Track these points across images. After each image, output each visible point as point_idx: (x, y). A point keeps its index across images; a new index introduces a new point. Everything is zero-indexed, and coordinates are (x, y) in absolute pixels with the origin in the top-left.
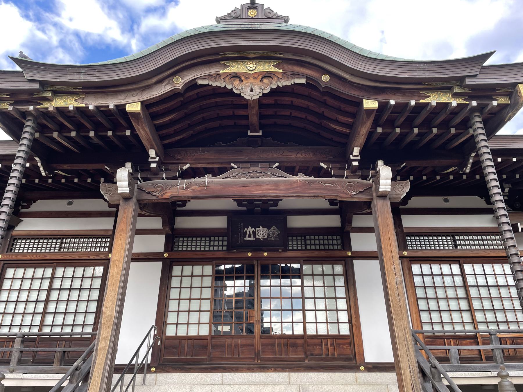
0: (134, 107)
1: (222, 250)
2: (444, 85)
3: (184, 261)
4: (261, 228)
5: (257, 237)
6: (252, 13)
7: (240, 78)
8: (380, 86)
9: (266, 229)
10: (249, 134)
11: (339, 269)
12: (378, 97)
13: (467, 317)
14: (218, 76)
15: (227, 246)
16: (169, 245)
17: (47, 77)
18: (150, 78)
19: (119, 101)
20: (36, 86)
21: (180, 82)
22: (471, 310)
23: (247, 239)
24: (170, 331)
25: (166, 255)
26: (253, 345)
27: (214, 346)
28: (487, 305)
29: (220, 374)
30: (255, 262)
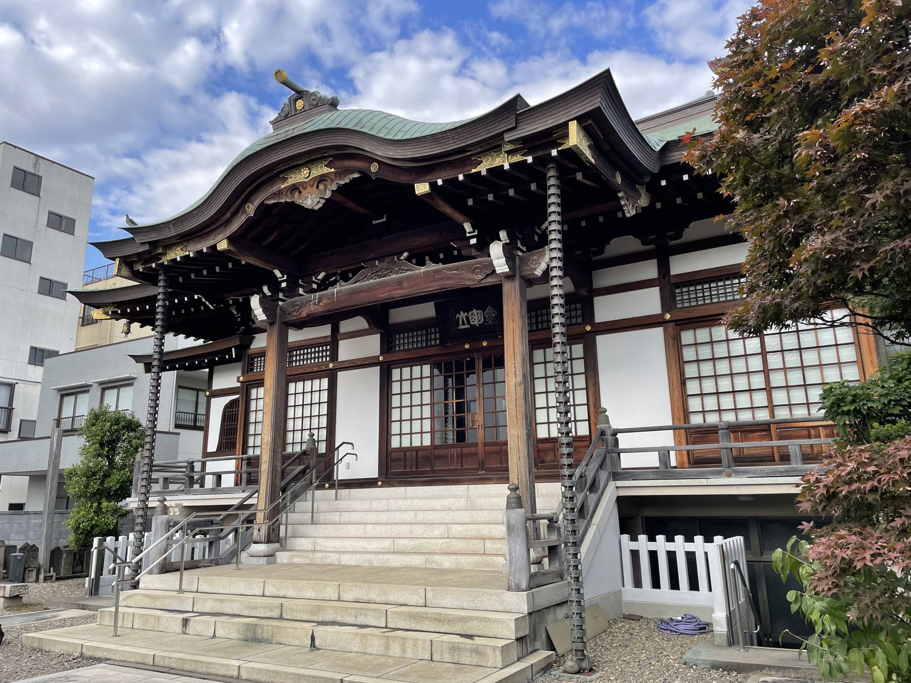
0: (223, 246)
1: (435, 345)
2: (493, 145)
4: (475, 311)
5: (472, 323)
6: (300, 104)
7: (298, 188)
8: (425, 167)
9: (480, 311)
10: (374, 222)
12: (428, 178)
13: (760, 399)
14: (280, 193)
15: (440, 339)
16: (387, 346)
17: (153, 237)
18: (225, 214)
19: (211, 243)
20: (147, 247)
21: (251, 209)
22: (768, 389)
23: (461, 327)
24: (395, 443)
25: (381, 358)
26: (476, 454)
27: (440, 457)
28: (795, 378)
29: (403, 488)
30: (475, 355)
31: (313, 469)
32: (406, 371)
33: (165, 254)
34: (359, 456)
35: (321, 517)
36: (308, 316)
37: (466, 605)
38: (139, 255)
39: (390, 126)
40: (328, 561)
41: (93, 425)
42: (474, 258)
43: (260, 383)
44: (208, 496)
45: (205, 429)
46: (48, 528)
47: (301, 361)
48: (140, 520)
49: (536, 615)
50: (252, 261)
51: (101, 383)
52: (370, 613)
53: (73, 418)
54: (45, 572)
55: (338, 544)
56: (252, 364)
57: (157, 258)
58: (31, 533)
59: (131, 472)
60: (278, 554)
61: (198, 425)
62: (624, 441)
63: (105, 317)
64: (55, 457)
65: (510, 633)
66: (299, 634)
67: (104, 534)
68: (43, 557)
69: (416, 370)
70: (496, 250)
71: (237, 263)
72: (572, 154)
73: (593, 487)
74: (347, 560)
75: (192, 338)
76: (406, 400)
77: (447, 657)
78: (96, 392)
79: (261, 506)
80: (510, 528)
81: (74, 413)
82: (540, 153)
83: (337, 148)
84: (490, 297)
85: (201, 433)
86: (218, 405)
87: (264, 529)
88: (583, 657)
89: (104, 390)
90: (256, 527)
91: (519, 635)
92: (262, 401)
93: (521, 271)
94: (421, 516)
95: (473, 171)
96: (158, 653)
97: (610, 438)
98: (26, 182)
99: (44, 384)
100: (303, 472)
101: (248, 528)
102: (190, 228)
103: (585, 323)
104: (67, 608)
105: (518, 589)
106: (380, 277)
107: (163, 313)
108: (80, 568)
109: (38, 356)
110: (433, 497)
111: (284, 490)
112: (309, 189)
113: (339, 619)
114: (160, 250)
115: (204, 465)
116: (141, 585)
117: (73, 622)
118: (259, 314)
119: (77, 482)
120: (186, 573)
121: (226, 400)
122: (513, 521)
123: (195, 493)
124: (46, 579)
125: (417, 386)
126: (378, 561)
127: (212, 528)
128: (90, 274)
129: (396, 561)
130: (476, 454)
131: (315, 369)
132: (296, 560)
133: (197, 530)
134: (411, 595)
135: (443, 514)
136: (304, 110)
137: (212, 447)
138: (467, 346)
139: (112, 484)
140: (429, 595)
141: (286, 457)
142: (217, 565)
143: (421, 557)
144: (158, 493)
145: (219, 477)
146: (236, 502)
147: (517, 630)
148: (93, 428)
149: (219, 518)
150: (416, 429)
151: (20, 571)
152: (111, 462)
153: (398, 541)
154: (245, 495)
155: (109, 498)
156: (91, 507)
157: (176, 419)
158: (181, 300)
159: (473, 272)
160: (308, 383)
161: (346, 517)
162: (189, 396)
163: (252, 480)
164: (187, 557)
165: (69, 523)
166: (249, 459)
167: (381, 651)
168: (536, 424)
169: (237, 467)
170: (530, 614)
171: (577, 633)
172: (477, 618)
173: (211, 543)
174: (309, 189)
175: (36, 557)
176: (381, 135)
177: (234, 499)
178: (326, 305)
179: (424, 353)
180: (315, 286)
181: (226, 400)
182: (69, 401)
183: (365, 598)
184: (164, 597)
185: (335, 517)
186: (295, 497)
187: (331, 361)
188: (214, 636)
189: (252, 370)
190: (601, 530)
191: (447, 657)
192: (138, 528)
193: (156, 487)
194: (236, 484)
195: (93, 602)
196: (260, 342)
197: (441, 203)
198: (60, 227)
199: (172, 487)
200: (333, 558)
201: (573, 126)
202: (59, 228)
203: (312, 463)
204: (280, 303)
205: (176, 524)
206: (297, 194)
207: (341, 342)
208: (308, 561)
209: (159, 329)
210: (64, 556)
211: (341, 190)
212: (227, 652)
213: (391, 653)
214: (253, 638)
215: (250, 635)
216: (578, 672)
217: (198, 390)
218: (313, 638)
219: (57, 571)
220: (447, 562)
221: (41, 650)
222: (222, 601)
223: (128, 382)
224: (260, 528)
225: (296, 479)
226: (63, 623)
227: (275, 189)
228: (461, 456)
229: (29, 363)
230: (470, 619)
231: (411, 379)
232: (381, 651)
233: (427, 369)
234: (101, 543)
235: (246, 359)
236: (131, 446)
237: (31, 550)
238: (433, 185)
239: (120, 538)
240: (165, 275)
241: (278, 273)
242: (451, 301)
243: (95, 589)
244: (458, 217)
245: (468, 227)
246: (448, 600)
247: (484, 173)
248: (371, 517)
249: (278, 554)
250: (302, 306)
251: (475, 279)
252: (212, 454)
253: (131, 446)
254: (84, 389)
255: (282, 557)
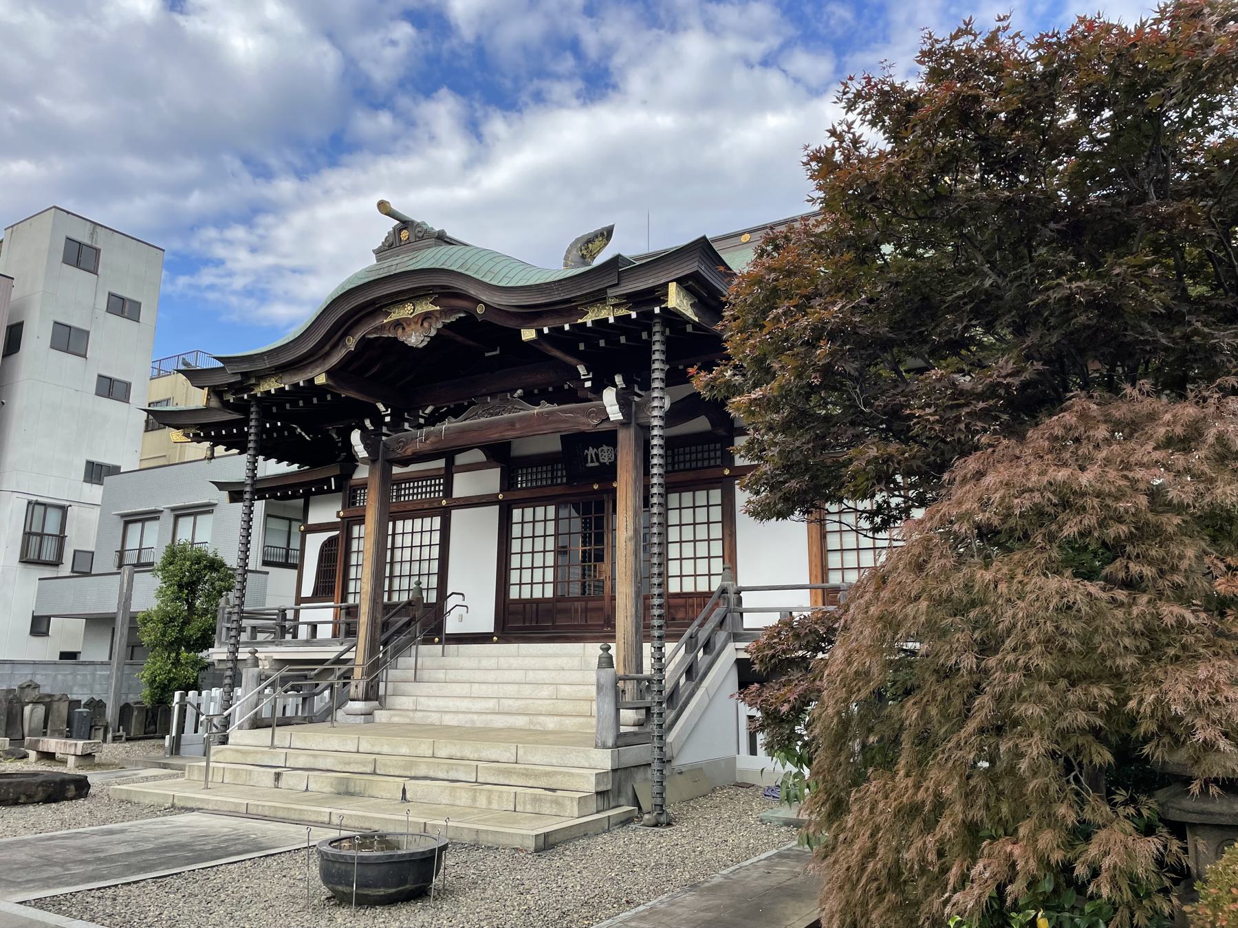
0: (321, 380)
2: (599, 298)
3: (523, 503)
4: (605, 448)
6: (405, 234)
8: (531, 315)
10: (487, 354)
11: (716, 495)
14: (383, 327)
16: (507, 482)
17: (246, 368)
19: (309, 376)
20: (239, 378)
21: (351, 343)
25: (501, 496)
26: (601, 609)
31: (420, 621)
32: (529, 512)
33: (258, 385)
34: (473, 607)
35: (425, 675)
36: (414, 454)
37: (554, 761)
38: (230, 385)
39: (496, 269)
40: (429, 721)
41: (171, 564)
42: (590, 400)
43: (361, 520)
44: (301, 649)
45: (299, 567)
46: (117, 681)
47: (411, 495)
48: (229, 673)
49: (620, 773)
50: (352, 395)
51: (173, 509)
52: (462, 768)
53: (140, 550)
54: (114, 731)
55: (441, 703)
56: (355, 497)
57: (249, 389)
58: (97, 687)
59: (215, 618)
60: (377, 713)
61: (290, 561)
62: (748, 600)
63: (185, 439)
64: (126, 599)
65: (590, 787)
66: (392, 788)
67: (186, 689)
68: (111, 713)
69: (540, 511)
70: (609, 396)
71: (336, 396)
72: (672, 317)
73: (707, 646)
74: (449, 720)
75: (286, 463)
76: (528, 545)
77: (529, 808)
78: (167, 518)
79: (359, 661)
80: (600, 688)
81: (141, 544)
82: (645, 309)
83: (441, 287)
84: (609, 438)
85: (295, 572)
86: (315, 543)
87: (362, 685)
88: (662, 812)
89: (177, 517)
90: (353, 683)
91: (600, 789)
92: (364, 538)
93: (636, 418)
94: (531, 676)
95: (580, 321)
96: (251, 802)
97: (733, 597)
98: (81, 255)
99: (104, 506)
100: (408, 624)
101: (345, 684)
102: (286, 361)
103: (723, 466)
104: (146, 767)
105: (604, 747)
106: (492, 415)
107: (255, 441)
108: (152, 727)
109: (96, 472)
110: (551, 656)
111: (385, 644)
112: (413, 326)
113: (431, 774)
114: (253, 381)
115: (297, 612)
116: (230, 741)
117: (155, 778)
118: (360, 451)
119: (153, 629)
120: (277, 729)
121: (325, 536)
122: (602, 681)
123: (288, 644)
124: (115, 739)
125: (538, 528)
126: (479, 721)
127: (309, 689)
128: (157, 365)
129: (499, 722)
130: (601, 609)
131: (426, 506)
132: (396, 719)
133: (288, 686)
134: (503, 753)
135: (554, 674)
136: (409, 241)
137: (307, 591)
138: (596, 487)
139: (193, 631)
140: (521, 752)
141: (388, 608)
142: (310, 722)
143: (527, 718)
144: (247, 644)
145: (314, 627)
146: (331, 656)
147: (597, 784)
148: (171, 567)
149: (313, 673)
150: (536, 581)
151: (85, 729)
152: (191, 606)
153: (502, 701)
154: (342, 648)
155: (189, 648)
156: (169, 657)
157: (264, 554)
158: (274, 425)
159: (588, 416)
160: (418, 522)
161: (452, 675)
162: (282, 525)
163: (351, 632)
164: (279, 714)
165: (142, 675)
166: (348, 608)
167: (469, 802)
168: (668, 577)
169: (336, 616)
170: (613, 770)
171: (657, 789)
172: (561, 773)
173: (304, 699)
174: (413, 326)
175: (103, 714)
176: (486, 280)
177: (330, 652)
178: (433, 443)
179: (549, 492)
180: (422, 421)
181: (325, 536)
182: (135, 529)
183: (459, 755)
184: (256, 752)
185: (440, 675)
186: (398, 651)
187: (445, 497)
188: (307, 789)
189: (354, 504)
190: (711, 693)
191: (529, 808)
192: (227, 681)
193: (244, 637)
194: (334, 636)
195: (175, 761)
196: (362, 473)
197: (549, 348)
198: (123, 312)
199: (261, 637)
200: (434, 718)
201: (673, 287)
202: (121, 314)
203: (418, 614)
204: (384, 438)
205: (267, 677)
206: (400, 331)
207: (456, 476)
208: (408, 721)
209: (251, 452)
210: (135, 713)
211: (445, 326)
212: (320, 802)
213: (478, 805)
214: (345, 792)
215: (342, 789)
216: (656, 825)
217: (290, 520)
218: (404, 791)
219: (127, 730)
220: (551, 723)
221: (129, 802)
222: (315, 756)
223: (206, 509)
224: (358, 684)
225: (399, 632)
226: (147, 779)
227: (377, 323)
228: (586, 610)
229: (85, 481)
230: (555, 773)
231: (534, 522)
232: (469, 802)
233: (551, 510)
234: (182, 697)
235: (350, 493)
236: (214, 589)
237: (97, 706)
238: (539, 332)
239: (204, 693)
240: (258, 406)
241: (381, 407)
242: (576, 442)
243: (176, 748)
244: (570, 360)
245: (582, 370)
246: (537, 757)
247: (589, 324)
248: (478, 676)
249: (377, 713)
250: (406, 444)
251: (591, 424)
252: (307, 600)
253: (214, 589)
254: (153, 515)
255: (381, 716)
